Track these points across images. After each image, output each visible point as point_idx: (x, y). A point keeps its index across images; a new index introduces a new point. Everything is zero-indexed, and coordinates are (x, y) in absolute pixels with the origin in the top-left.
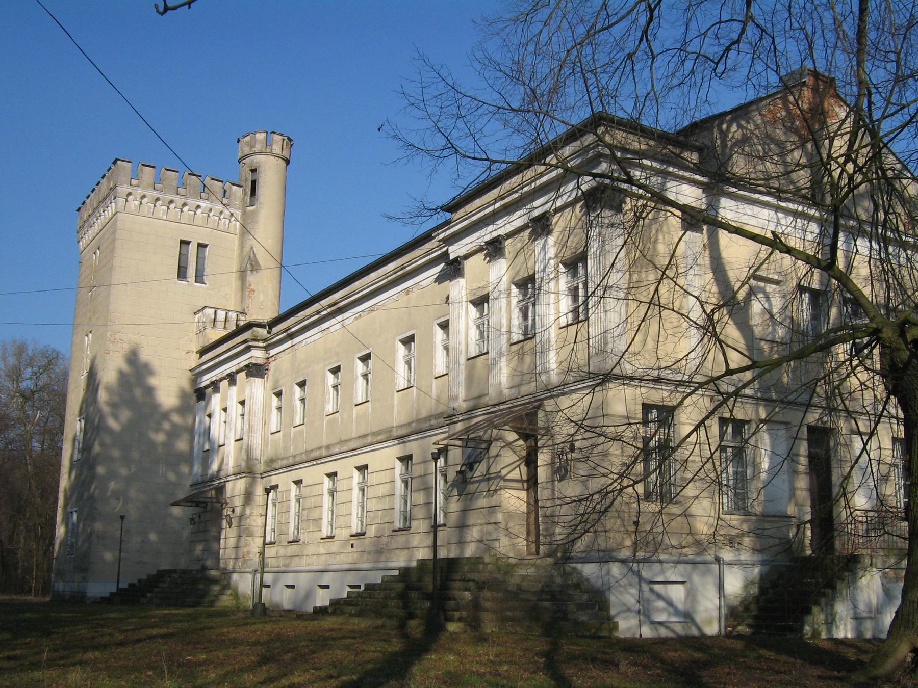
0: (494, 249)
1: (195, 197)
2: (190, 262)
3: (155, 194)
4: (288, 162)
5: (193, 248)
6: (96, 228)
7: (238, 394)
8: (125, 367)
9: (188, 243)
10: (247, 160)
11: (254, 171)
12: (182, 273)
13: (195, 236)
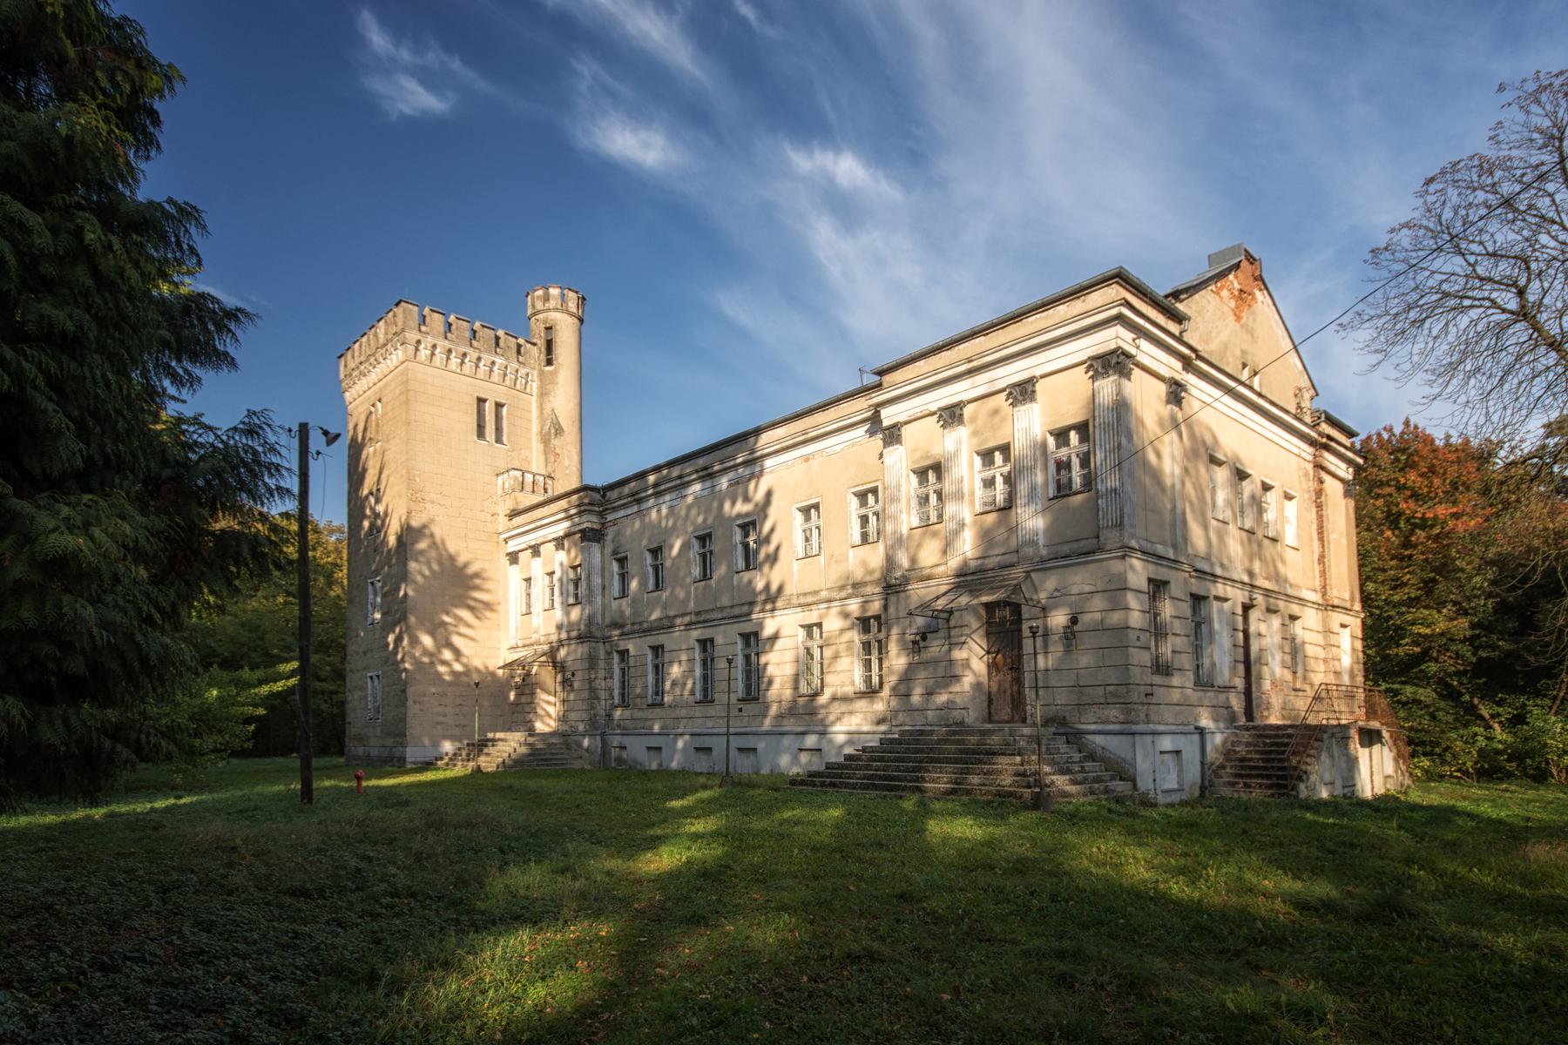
0: (952, 415)
1: (489, 352)
2: (488, 420)
3: (447, 344)
4: (581, 321)
5: (489, 408)
6: (373, 377)
7: (545, 564)
8: (1448, 333)
9: (484, 401)
10: (541, 316)
11: (549, 329)
12: (481, 433)
13: (494, 393)
